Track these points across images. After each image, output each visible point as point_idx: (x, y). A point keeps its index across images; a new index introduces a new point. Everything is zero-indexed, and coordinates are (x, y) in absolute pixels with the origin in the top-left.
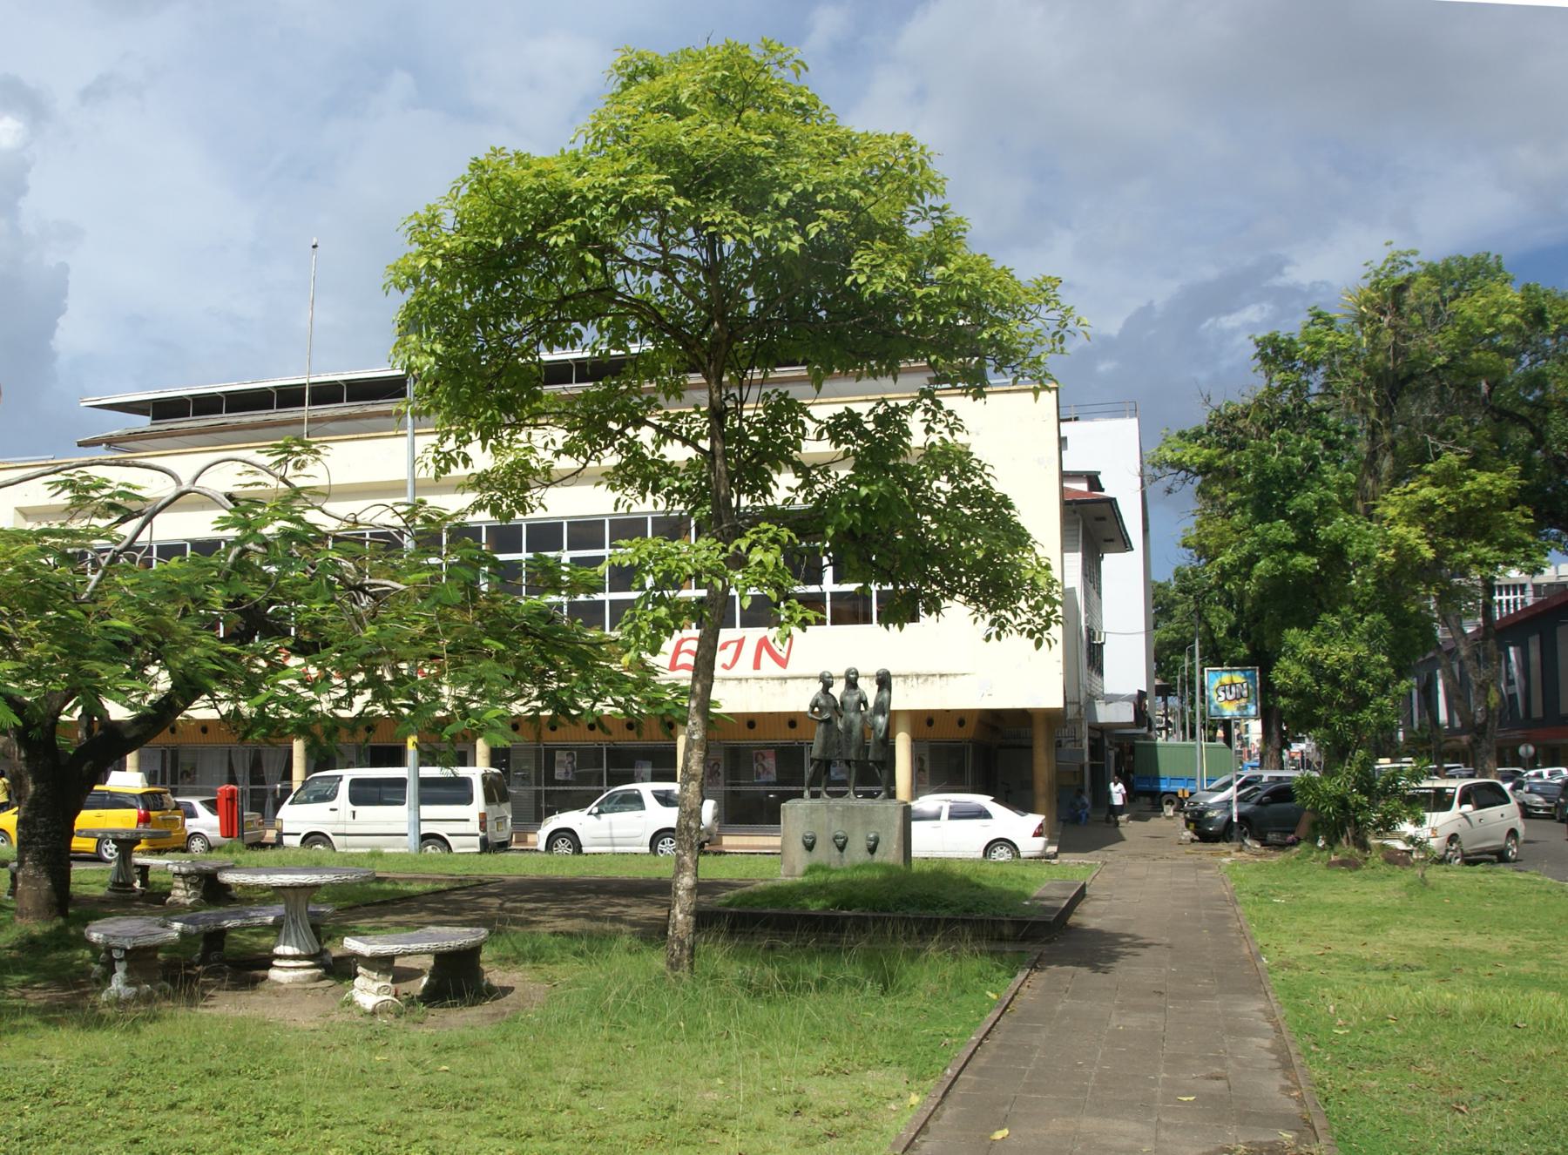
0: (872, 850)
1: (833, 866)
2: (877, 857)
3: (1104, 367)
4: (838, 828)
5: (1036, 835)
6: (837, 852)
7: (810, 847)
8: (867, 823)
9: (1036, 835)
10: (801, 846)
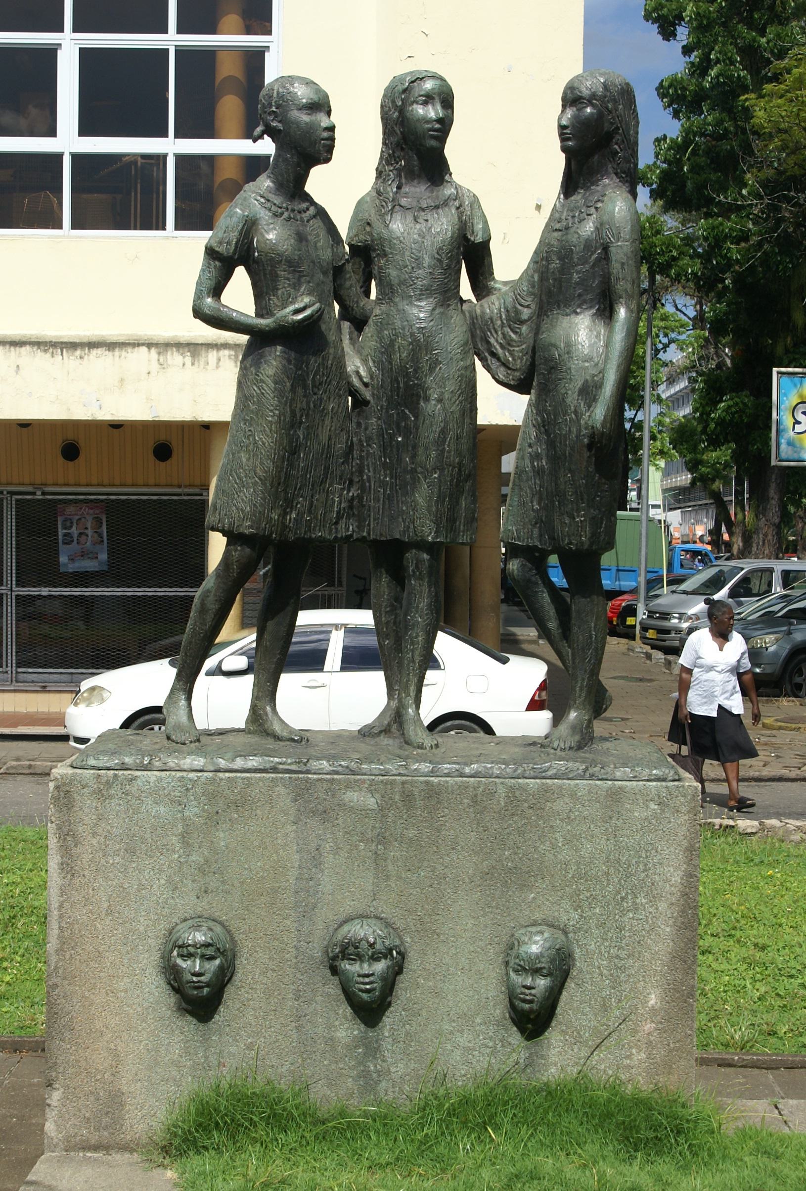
0: (533, 1020)
1: (325, 1095)
2: (560, 1056)
3: (537, 554)
4: (351, 897)
5: (534, 705)
6: (346, 1028)
7: (200, 1003)
8: (509, 876)
9: (534, 705)
10: (154, 990)
